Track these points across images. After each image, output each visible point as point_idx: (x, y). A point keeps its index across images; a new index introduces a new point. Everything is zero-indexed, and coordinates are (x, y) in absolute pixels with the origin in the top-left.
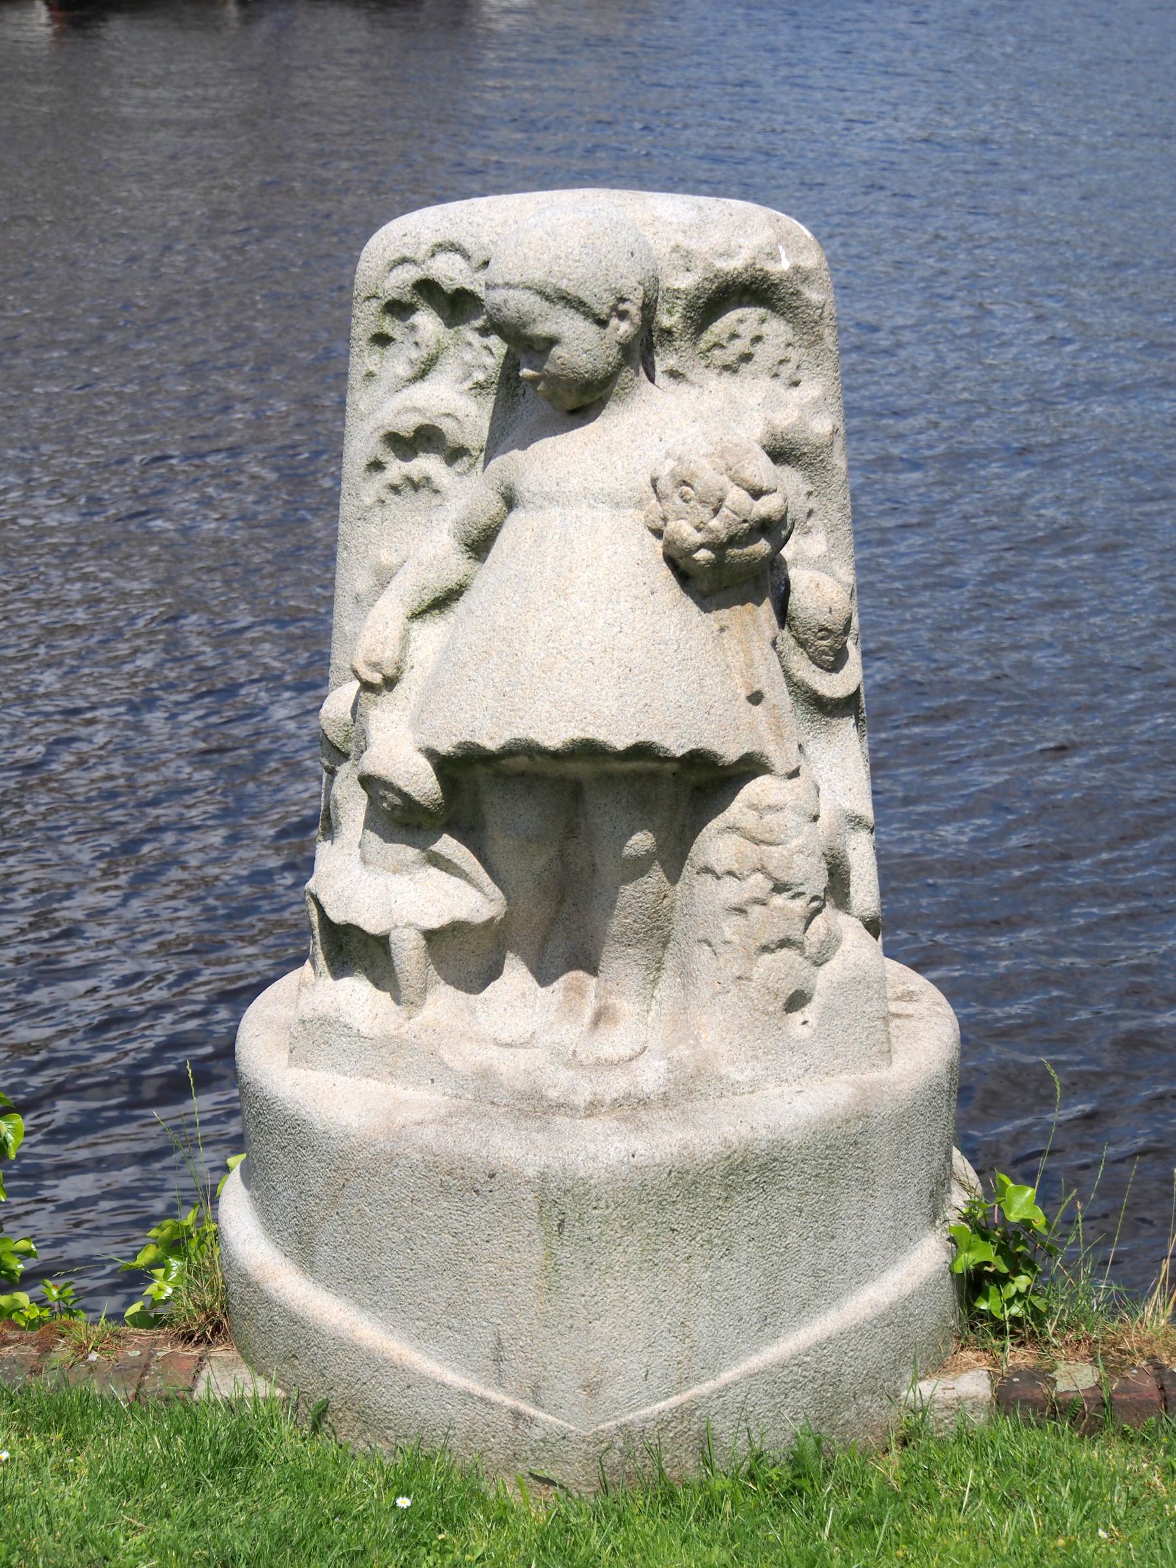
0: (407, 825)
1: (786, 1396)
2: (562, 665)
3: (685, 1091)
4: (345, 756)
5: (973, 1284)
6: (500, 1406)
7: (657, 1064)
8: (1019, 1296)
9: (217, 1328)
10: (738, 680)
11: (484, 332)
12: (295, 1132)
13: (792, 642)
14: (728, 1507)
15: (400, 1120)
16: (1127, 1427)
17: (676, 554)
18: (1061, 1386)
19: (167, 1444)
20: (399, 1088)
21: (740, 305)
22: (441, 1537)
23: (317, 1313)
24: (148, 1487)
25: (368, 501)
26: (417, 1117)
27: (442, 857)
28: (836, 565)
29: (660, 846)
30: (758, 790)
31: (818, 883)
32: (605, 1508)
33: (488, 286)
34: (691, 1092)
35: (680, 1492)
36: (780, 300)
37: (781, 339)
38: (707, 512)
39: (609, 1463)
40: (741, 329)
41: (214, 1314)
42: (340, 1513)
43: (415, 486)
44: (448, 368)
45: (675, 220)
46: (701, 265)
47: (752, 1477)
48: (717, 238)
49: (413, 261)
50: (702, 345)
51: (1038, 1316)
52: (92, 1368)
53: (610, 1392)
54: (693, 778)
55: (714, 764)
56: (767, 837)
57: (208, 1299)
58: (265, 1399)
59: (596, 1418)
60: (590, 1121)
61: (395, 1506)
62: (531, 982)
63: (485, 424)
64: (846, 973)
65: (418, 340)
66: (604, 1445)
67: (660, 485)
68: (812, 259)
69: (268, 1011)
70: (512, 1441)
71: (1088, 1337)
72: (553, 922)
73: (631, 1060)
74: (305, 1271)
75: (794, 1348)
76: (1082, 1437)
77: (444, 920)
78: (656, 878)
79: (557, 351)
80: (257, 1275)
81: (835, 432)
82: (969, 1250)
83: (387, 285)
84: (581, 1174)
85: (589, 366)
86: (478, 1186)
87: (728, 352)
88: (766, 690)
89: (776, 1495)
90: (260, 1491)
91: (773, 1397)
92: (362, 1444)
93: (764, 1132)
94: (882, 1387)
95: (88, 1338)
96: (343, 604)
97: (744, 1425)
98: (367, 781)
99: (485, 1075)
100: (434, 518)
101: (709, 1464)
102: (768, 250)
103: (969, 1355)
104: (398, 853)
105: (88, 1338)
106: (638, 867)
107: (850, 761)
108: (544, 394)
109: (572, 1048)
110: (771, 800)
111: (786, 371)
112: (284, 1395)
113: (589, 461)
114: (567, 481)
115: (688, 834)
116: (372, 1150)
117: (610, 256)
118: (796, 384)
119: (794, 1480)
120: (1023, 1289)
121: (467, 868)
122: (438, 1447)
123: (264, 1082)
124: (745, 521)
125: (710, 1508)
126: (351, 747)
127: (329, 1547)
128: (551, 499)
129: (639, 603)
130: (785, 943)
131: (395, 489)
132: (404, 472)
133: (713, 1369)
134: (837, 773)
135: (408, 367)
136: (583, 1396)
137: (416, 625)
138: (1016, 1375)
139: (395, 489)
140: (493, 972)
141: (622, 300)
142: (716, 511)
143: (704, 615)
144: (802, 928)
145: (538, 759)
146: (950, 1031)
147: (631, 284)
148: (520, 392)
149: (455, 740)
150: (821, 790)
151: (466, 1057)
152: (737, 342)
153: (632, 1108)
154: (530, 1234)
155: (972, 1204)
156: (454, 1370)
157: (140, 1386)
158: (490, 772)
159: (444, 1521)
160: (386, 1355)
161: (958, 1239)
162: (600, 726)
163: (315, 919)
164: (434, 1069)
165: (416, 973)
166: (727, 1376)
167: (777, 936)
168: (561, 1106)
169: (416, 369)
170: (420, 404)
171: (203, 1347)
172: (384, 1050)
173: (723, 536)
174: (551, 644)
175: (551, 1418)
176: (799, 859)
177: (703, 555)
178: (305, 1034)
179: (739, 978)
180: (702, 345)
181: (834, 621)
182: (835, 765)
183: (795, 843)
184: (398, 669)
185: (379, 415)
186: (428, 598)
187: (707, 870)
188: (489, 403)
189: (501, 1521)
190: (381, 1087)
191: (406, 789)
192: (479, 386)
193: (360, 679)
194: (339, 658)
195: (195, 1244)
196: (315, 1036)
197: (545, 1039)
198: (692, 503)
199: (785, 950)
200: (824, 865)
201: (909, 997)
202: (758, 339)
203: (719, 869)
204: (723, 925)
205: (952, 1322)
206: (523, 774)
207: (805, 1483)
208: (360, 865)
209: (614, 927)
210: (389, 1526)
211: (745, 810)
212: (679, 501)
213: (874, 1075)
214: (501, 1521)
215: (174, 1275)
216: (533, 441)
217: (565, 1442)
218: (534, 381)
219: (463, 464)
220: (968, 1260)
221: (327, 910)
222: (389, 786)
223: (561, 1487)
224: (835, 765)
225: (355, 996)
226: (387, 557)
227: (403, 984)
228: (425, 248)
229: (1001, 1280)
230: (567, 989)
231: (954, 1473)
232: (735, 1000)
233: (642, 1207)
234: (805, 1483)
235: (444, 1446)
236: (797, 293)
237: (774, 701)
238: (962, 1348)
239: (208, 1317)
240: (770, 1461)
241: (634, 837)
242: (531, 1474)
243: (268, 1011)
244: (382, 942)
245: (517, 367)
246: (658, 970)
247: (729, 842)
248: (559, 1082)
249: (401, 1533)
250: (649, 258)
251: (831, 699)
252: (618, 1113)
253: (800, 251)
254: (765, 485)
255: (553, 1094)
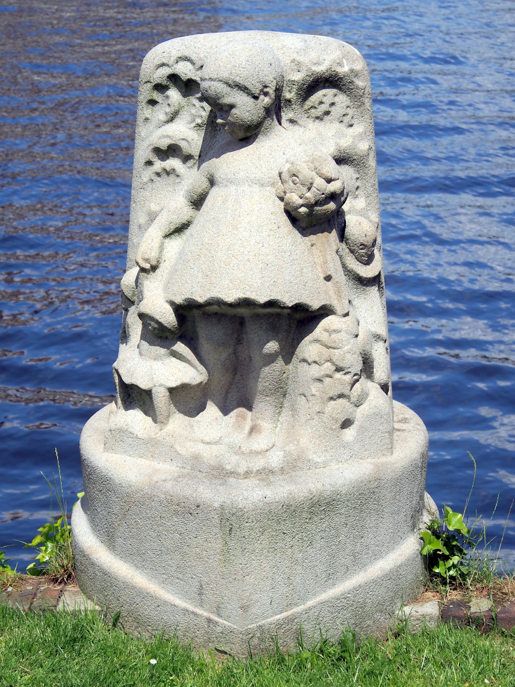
0: (161, 337)
1: (339, 613)
2: (234, 262)
3: (292, 466)
4: (133, 303)
5: (431, 560)
6: (202, 616)
7: (279, 453)
8: (454, 566)
9: (69, 576)
10: (320, 270)
11: (201, 99)
12: (106, 484)
13: (347, 250)
14: (309, 665)
15: (155, 479)
16: (504, 630)
17: (290, 209)
18: (473, 610)
19: (43, 633)
20: (156, 463)
21: (324, 88)
22: (171, 678)
23: (116, 570)
24: (33, 652)
25: (145, 180)
26: (163, 478)
27: (178, 353)
28: (370, 213)
29: (282, 347)
30: (329, 322)
31: (358, 367)
32: (250, 665)
33: (202, 79)
34: (295, 467)
35: (287, 658)
36: (344, 85)
37: (344, 104)
38: (305, 189)
39: (253, 644)
40: (324, 99)
41: (68, 570)
42: (124, 666)
43: (168, 173)
44: (184, 116)
45: (293, 47)
46: (305, 69)
47: (322, 651)
48: (313, 55)
49: (168, 65)
50: (306, 107)
51: (463, 575)
52: (9, 595)
53: (254, 610)
54: (298, 316)
55: (307, 310)
56: (333, 345)
57: (65, 562)
58: (91, 611)
59: (247, 622)
60: (246, 480)
61: (149, 663)
62: (218, 413)
63: (200, 143)
64: (371, 411)
65: (170, 103)
66: (251, 635)
67: (283, 176)
68: (359, 65)
69: (96, 424)
70: (207, 633)
71: (487, 586)
72: (231, 384)
73: (267, 451)
74: (110, 550)
75: (343, 590)
76: (482, 634)
77: (178, 383)
78: (279, 363)
79: (234, 111)
80: (88, 552)
81: (370, 149)
82: (430, 543)
83: (155, 76)
84: (240, 506)
85: (250, 118)
86: (192, 512)
87: (318, 110)
88: (333, 275)
89: (333, 660)
90: (86, 655)
91: (332, 613)
92: (136, 633)
93: (329, 487)
94: (386, 609)
95: (8, 580)
96: (133, 228)
97: (318, 626)
98: (141, 316)
99: (196, 457)
100: (176, 188)
101: (301, 645)
102: (338, 61)
103: (429, 594)
104: (157, 351)
105: (8, 580)
106: (271, 359)
107: (375, 308)
108: (229, 131)
109: (239, 445)
110: (335, 327)
111: (346, 119)
112: (100, 609)
113: (249, 164)
114: (238, 173)
115: (296, 343)
116: (142, 493)
117: (260, 66)
118: (351, 126)
119: (341, 653)
120: (456, 563)
121: (190, 358)
122: (172, 635)
123: (92, 459)
124: (323, 194)
125: (301, 666)
126: (135, 298)
127: (118, 682)
128: (231, 182)
129: (272, 233)
130: (341, 396)
131: (158, 174)
132: (163, 166)
133: (303, 600)
134: (370, 313)
135: (165, 116)
136: (241, 612)
137: (167, 240)
138: (451, 604)
139: (158, 174)
140: (202, 408)
141: (266, 87)
142: (309, 189)
143: (304, 238)
144: (349, 389)
145: (223, 307)
146: (423, 438)
147: (270, 79)
148: (218, 129)
149: (183, 297)
150: (363, 320)
151: (187, 449)
152: (322, 106)
153: (266, 474)
154: (216, 534)
155: (433, 522)
156: (180, 598)
157: (31, 604)
158: (201, 312)
159: (173, 671)
160: (148, 591)
161: (424, 538)
162: (252, 292)
163: (117, 381)
164: (173, 455)
165: (164, 408)
166: (310, 603)
167: (337, 392)
168: (233, 473)
169: (169, 117)
170: (170, 134)
171: (63, 585)
172: (149, 445)
173: (313, 201)
174: (229, 252)
175: (225, 622)
176: (348, 356)
177: (303, 210)
178: (111, 436)
179: (319, 412)
180: (306, 107)
181: (368, 241)
182: (368, 310)
183: (346, 348)
184: (158, 262)
185: (151, 138)
186: (173, 228)
187: (304, 360)
188: (202, 134)
189: (200, 671)
190: (147, 462)
191: (160, 320)
192: (198, 125)
193: (139, 266)
194: (130, 255)
195: (59, 534)
196: (116, 437)
197: (226, 440)
198: (298, 185)
199: (341, 399)
200: (361, 358)
201: (405, 420)
202: (333, 104)
203: (310, 360)
204: (312, 387)
205: (421, 578)
206: (216, 314)
207: (346, 655)
208: (138, 356)
209: (260, 387)
210: (147, 674)
211: (323, 332)
212: (292, 184)
213: (383, 460)
214: (200, 671)
215: (49, 550)
216: (223, 153)
217: (232, 634)
218: (223, 125)
219: (191, 163)
220: (429, 548)
221: (122, 377)
222: (152, 319)
223: (230, 655)
224: (368, 310)
225: (135, 419)
226: (154, 207)
227: (158, 413)
228: (173, 59)
229: (446, 558)
230: (237, 416)
231: (419, 651)
232: (317, 423)
233: (269, 522)
234: (346, 655)
235: (175, 635)
236: (352, 82)
237: (337, 280)
238: (426, 590)
239: (65, 571)
240: (331, 644)
241: (268, 344)
242: (216, 649)
243: (96, 424)
244: (149, 393)
245: (216, 117)
246: (281, 407)
247: (315, 347)
248: (231, 462)
249: (152, 676)
250: (279, 66)
251: (366, 278)
252: (259, 477)
253: (354, 61)
254: (333, 176)
255: (228, 467)
